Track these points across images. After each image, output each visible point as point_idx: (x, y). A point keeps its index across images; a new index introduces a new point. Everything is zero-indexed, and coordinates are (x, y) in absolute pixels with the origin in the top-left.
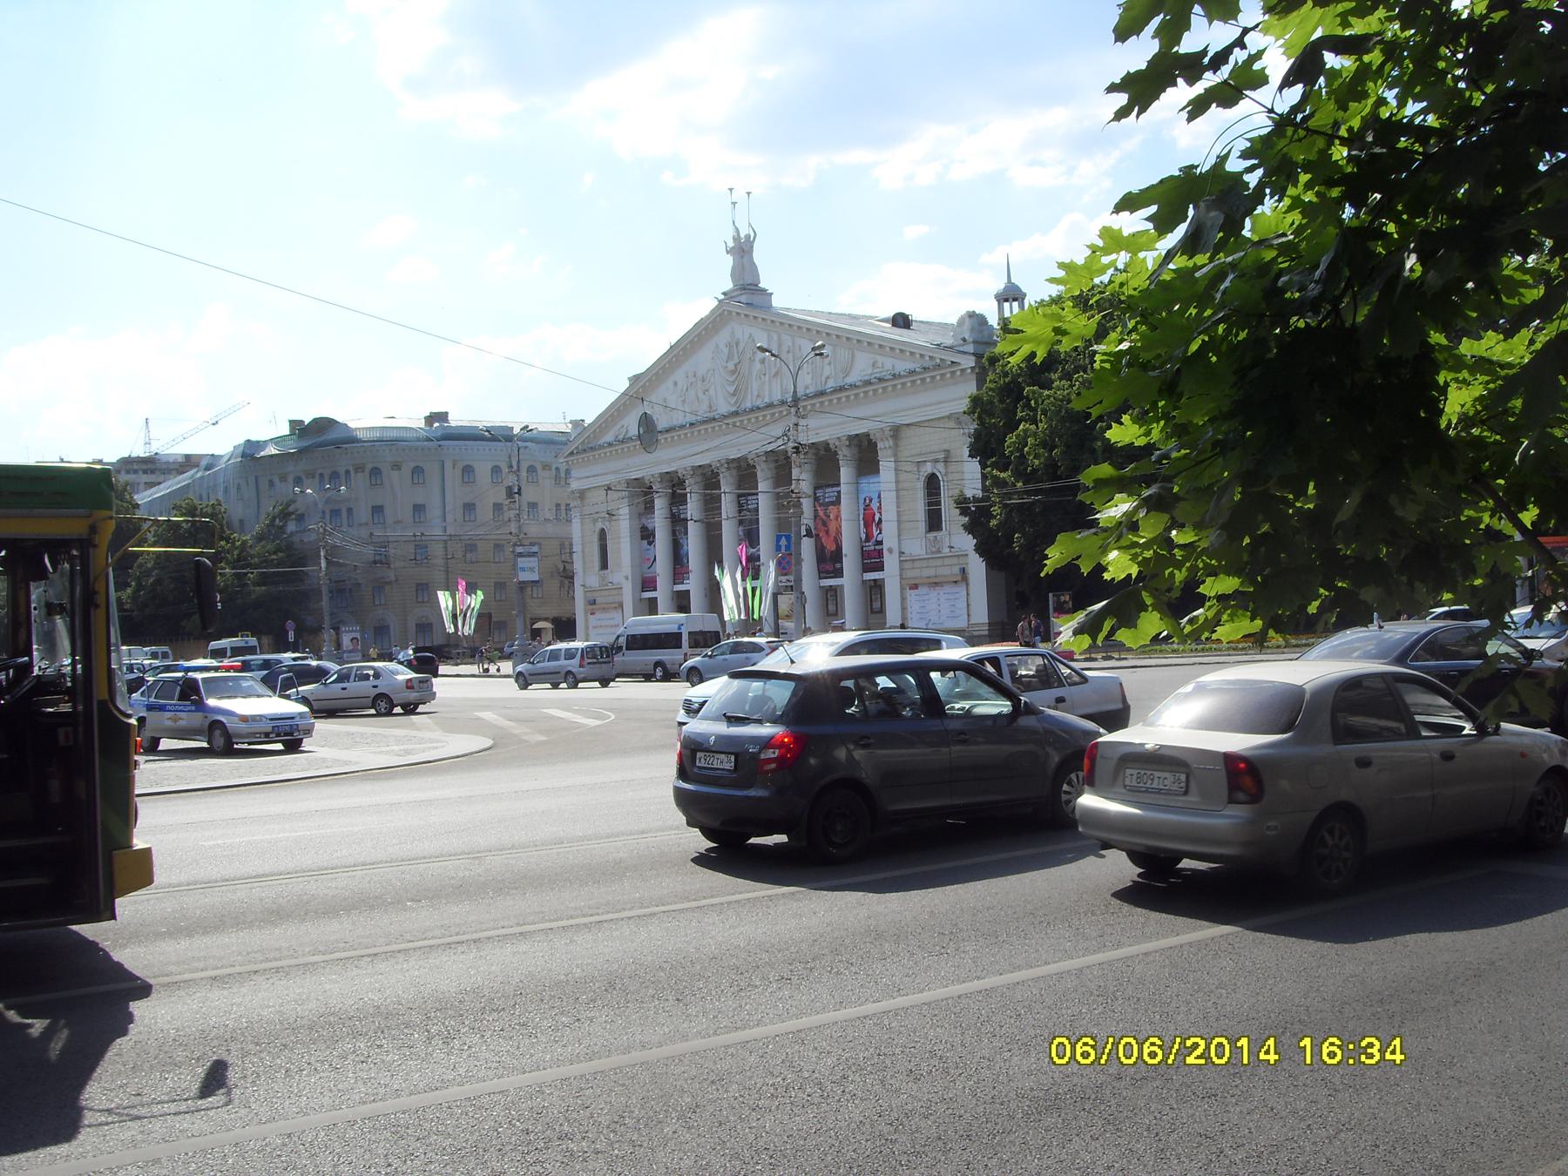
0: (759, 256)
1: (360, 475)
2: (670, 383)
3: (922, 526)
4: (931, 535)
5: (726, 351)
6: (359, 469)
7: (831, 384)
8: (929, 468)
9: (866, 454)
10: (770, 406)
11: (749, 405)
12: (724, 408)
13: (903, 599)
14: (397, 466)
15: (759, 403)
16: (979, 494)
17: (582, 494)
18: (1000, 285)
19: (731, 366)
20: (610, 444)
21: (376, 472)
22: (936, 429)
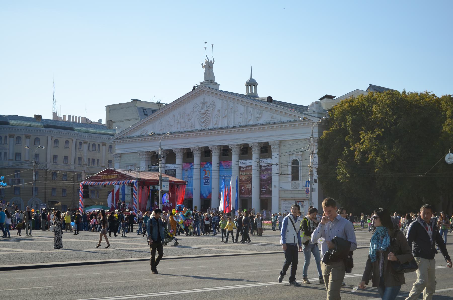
0: (215, 70)
1: (12, 139)
2: (171, 115)
3: (290, 177)
4: (294, 182)
5: (201, 105)
6: (11, 136)
7: (251, 123)
8: (294, 157)
9: (265, 150)
10: (221, 128)
11: (210, 127)
12: (198, 127)
13: (280, 205)
14: (28, 137)
15: (216, 126)
16: (141, 162)
17: (121, 155)
18: (248, 78)
19: (203, 111)
20: (137, 137)
21: (19, 138)
22: (304, 143)
